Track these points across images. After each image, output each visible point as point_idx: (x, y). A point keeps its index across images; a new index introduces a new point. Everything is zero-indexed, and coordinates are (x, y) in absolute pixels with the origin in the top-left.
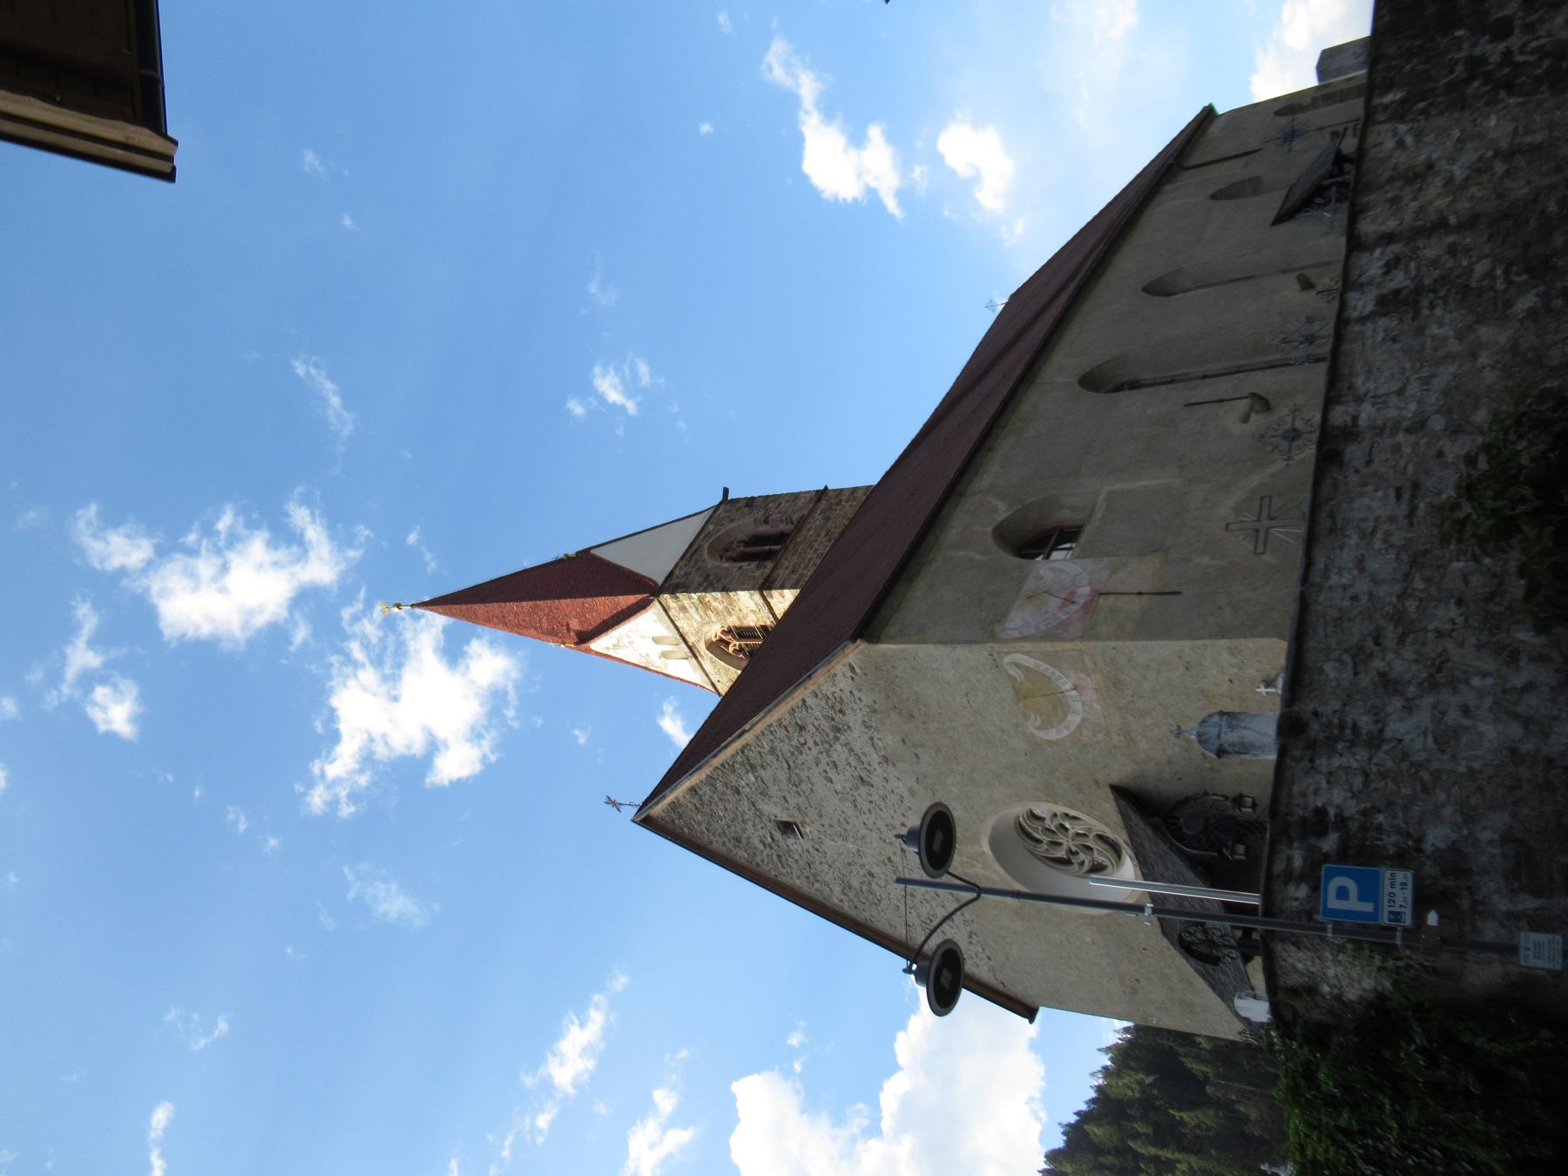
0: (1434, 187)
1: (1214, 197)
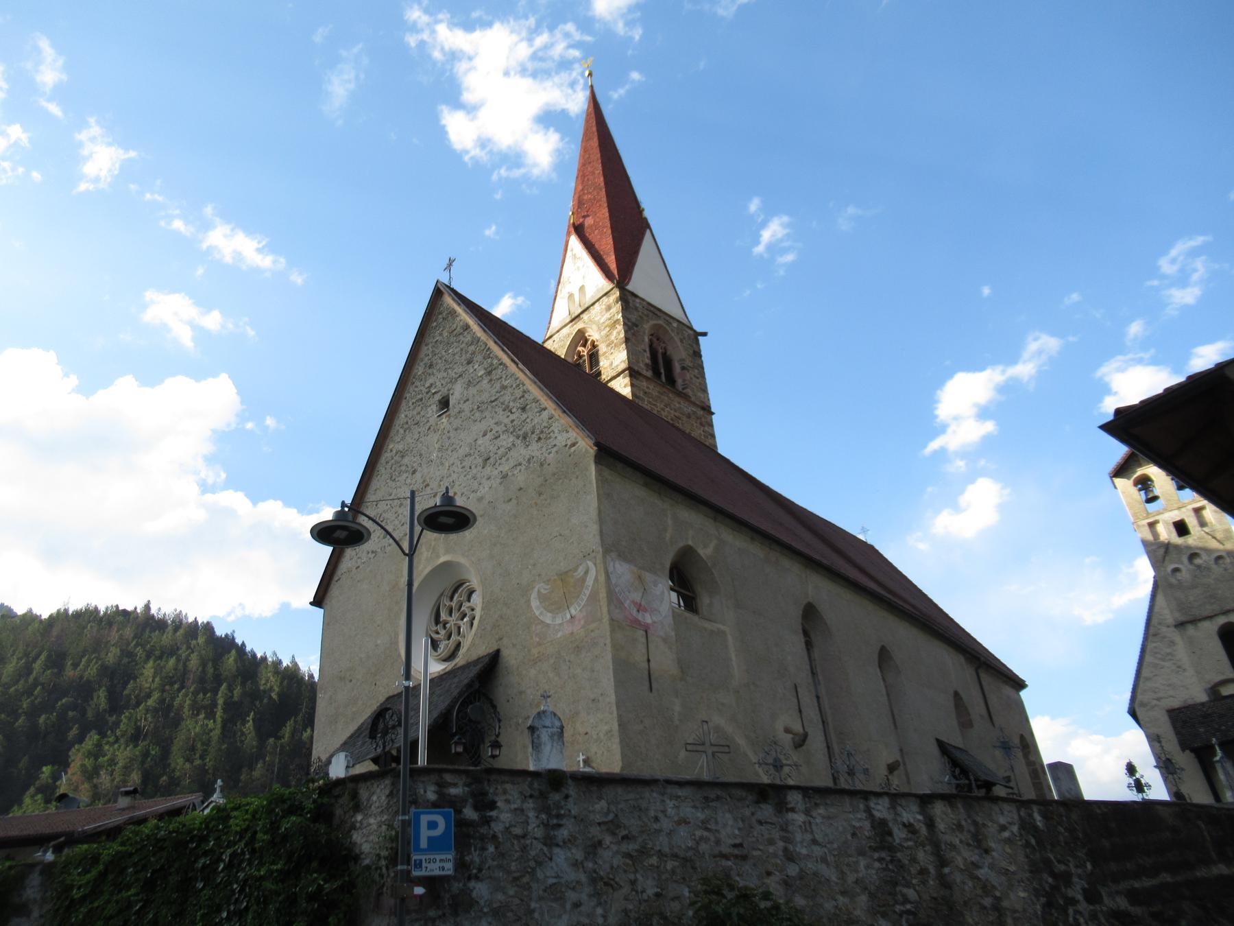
0: (972, 855)
1: (956, 694)
